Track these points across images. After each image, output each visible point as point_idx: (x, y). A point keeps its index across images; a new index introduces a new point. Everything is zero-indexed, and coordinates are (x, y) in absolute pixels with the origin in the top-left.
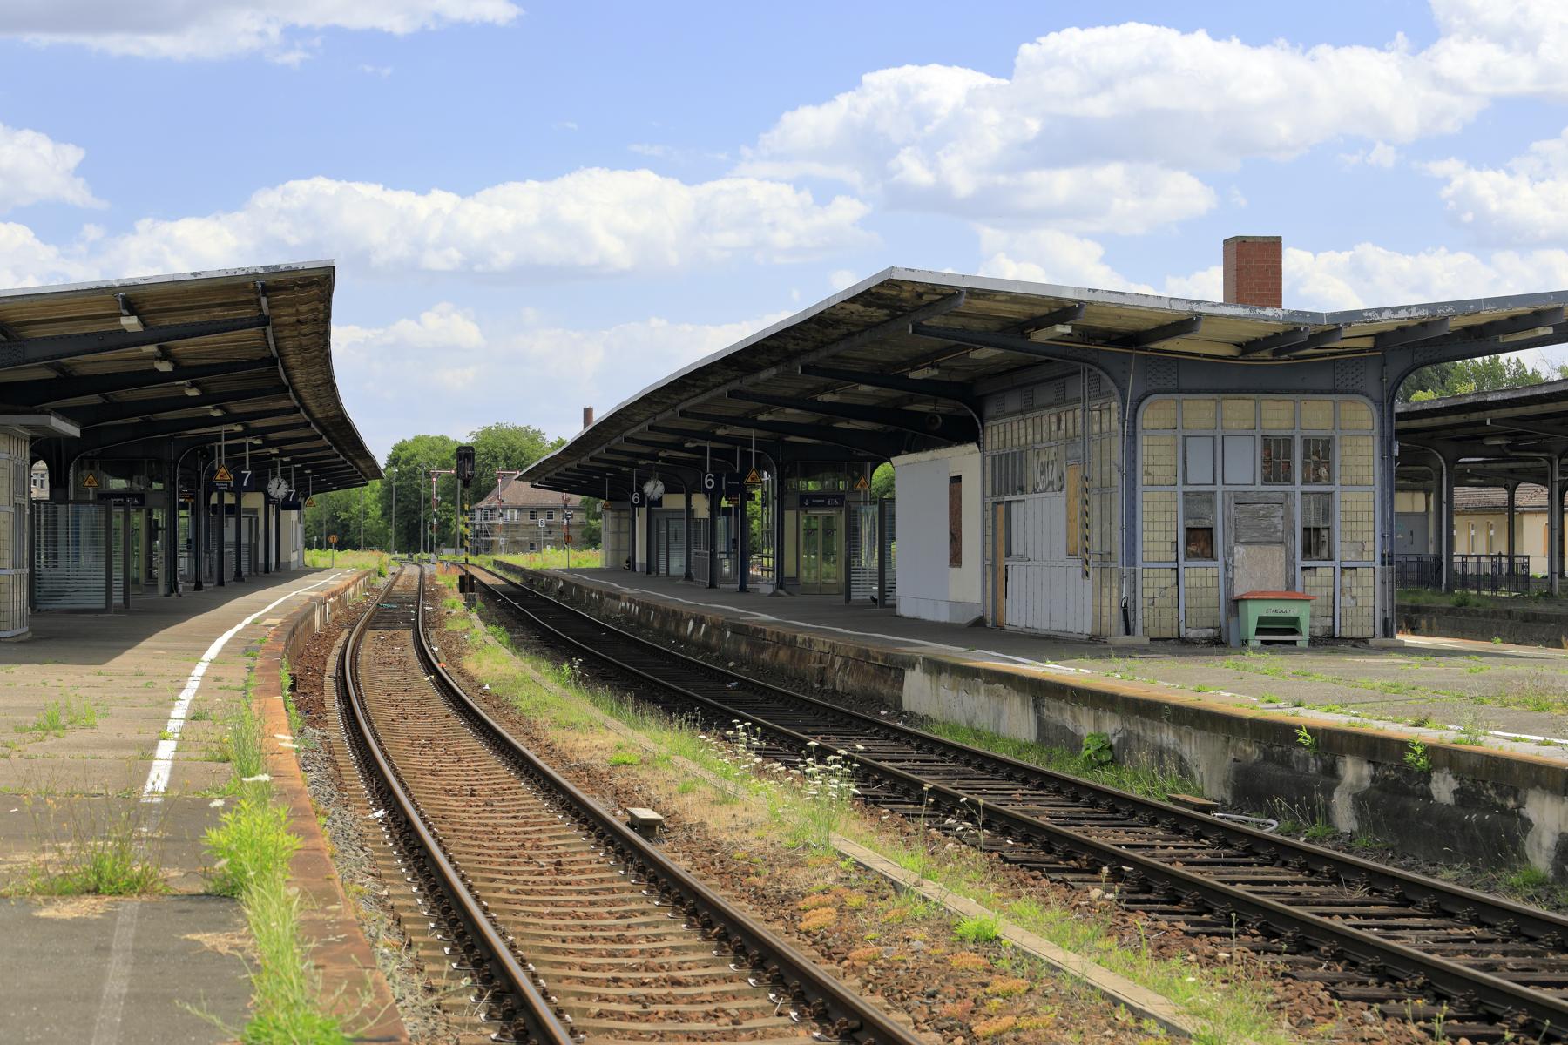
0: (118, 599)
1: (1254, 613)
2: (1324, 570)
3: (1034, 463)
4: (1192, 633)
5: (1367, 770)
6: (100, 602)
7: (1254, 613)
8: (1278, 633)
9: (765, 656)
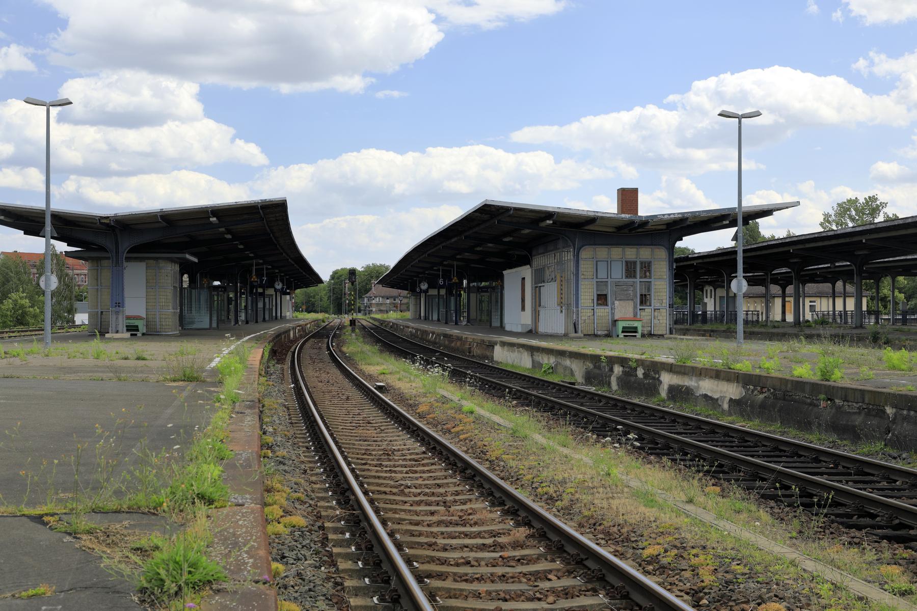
0: (214, 325)
1: (621, 325)
2: (648, 310)
3: (547, 272)
4: (599, 333)
5: (621, 369)
6: (207, 326)
7: (621, 325)
8: (630, 332)
9: (453, 345)
